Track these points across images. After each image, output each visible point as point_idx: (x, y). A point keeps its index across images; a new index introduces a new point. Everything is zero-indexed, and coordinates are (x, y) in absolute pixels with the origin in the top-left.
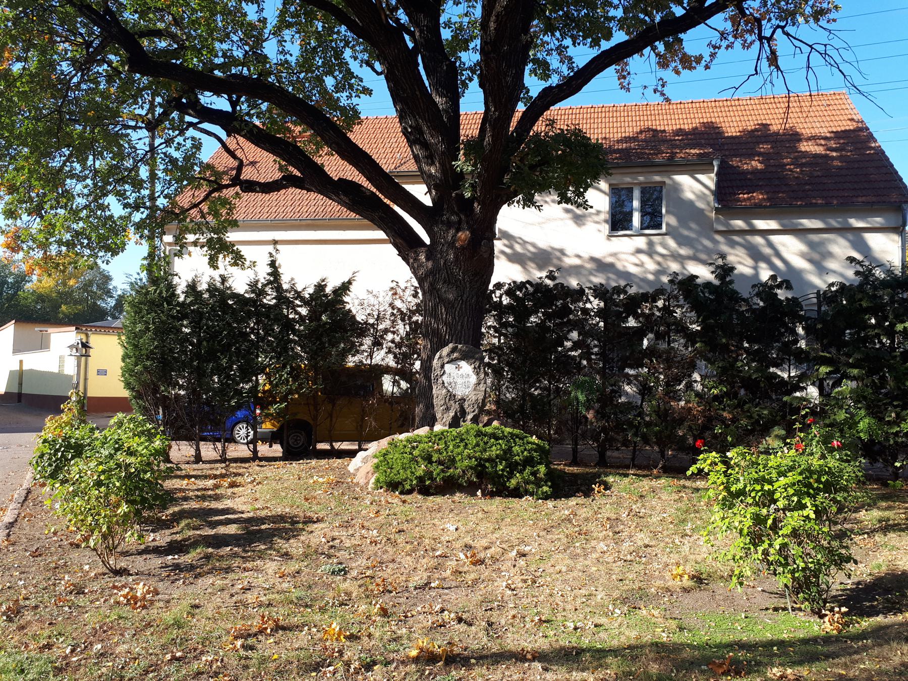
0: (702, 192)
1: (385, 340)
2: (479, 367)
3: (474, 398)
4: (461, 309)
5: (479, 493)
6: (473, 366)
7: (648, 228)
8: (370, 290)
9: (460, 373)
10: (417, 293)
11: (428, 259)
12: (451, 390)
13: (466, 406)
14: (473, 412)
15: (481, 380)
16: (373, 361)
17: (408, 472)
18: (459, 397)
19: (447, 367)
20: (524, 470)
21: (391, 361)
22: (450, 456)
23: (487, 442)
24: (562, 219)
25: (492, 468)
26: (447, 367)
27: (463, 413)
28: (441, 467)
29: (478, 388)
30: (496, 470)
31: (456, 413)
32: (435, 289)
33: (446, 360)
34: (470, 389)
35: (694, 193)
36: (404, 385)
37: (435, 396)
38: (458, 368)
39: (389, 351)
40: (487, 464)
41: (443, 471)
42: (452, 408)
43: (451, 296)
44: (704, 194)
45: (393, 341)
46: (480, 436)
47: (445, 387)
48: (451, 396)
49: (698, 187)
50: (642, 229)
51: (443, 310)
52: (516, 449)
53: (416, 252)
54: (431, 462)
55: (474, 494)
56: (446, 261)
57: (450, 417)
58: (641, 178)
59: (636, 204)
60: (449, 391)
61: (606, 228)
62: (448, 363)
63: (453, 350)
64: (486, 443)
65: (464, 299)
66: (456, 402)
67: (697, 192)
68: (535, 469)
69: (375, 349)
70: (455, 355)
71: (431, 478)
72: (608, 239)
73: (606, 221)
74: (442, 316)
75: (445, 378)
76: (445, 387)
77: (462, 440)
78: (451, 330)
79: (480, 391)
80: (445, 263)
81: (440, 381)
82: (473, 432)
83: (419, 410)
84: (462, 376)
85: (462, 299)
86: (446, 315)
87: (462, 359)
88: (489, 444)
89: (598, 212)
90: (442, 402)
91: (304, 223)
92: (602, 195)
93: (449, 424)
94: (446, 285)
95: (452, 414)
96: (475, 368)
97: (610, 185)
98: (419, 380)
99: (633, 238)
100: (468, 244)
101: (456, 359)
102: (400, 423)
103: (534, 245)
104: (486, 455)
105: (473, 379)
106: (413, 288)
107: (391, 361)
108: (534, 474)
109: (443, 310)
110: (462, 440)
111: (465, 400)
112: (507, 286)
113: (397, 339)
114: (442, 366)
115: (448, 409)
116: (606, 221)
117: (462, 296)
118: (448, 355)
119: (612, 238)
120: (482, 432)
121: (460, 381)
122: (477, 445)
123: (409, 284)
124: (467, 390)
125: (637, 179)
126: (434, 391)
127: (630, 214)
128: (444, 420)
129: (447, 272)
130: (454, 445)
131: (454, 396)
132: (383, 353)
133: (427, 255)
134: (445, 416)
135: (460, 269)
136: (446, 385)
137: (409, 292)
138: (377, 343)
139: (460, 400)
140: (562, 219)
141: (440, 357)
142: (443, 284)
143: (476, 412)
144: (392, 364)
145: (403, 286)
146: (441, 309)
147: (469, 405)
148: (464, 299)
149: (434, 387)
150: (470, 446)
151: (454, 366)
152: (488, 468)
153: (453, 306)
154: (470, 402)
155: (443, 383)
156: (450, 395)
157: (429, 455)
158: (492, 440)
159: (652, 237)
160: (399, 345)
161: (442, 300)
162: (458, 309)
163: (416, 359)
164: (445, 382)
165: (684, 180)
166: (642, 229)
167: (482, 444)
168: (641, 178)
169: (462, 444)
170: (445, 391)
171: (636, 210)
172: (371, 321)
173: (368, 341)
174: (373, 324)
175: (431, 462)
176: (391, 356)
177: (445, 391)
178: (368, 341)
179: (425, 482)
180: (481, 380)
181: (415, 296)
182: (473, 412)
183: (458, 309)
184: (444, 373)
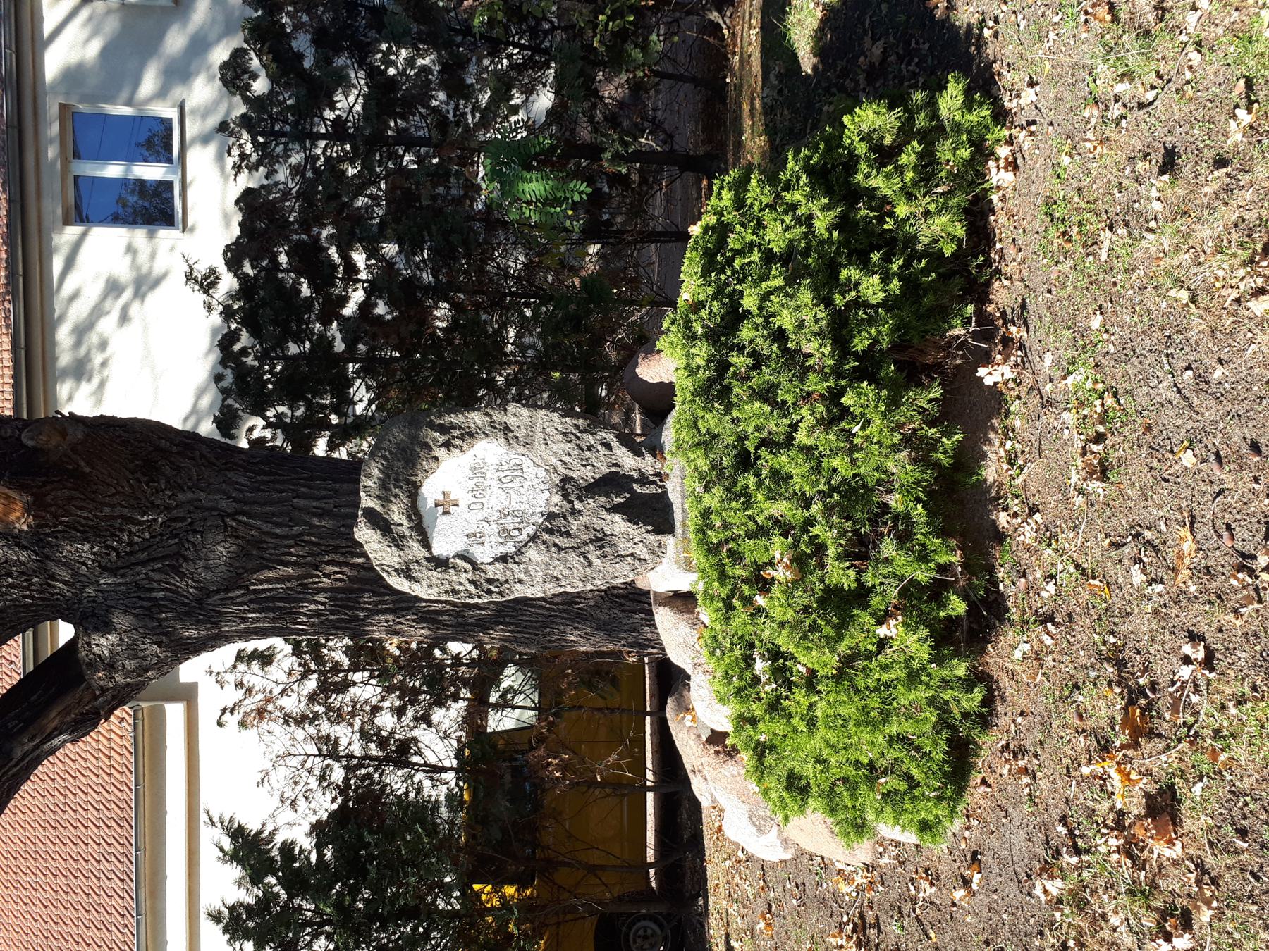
0: (85, 25)
1: (393, 732)
2: (443, 429)
3: (559, 446)
4: (266, 518)
5: (989, 376)
6: (440, 452)
7: (168, 147)
8: (259, 777)
9: (464, 499)
10: (255, 656)
11: (106, 627)
12: (530, 530)
13: (588, 475)
14: (608, 446)
15: (492, 424)
16: (447, 764)
17: (904, 698)
18: (557, 498)
19: (441, 547)
20: (871, 193)
21: (449, 716)
22: (828, 511)
23: (754, 354)
24: (145, 328)
25: (872, 321)
26: (441, 547)
27: (611, 483)
28: (888, 548)
29: (521, 433)
30: (884, 304)
31: (615, 509)
32: (199, 601)
33: (417, 551)
34: (527, 463)
35: (88, 40)
36: (511, 677)
37: (551, 589)
38: (446, 506)
39: (426, 719)
40: (860, 344)
41: (904, 538)
42: (598, 524)
43: (223, 551)
44: (90, 19)
45: (399, 712)
46: (727, 390)
47: (519, 552)
48: (553, 525)
49: (75, 30)
50: (170, 161)
51: (272, 574)
52: (776, 235)
53: (90, 665)
54: (861, 595)
55: (995, 400)
56: (103, 568)
57: (631, 529)
58: (52, 152)
59: (114, 170)
60: (533, 538)
61: (164, 234)
62: (426, 544)
63: (380, 523)
64: (759, 361)
65: (230, 507)
66: (574, 512)
67: (85, 34)
68: (861, 149)
69: (416, 759)
70: (397, 515)
71: (937, 591)
72: (192, 230)
73: (151, 235)
74: (289, 578)
75: (483, 554)
76: (519, 552)
77: (745, 462)
78: (336, 549)
79: (532, 427)
80: (113, 571)
81: (495, 571)
82: (711, 421)
83: (581, 642)
84: (477, 491)
85: (232, 516)
86: (286, 564)
87: (414, 492)
88: (763, 346)
89: (131, 250)
90: (574, 559)
91: (146, 905)
92: (89, 240)
93: (657, 531)
94: (186, 567)
95: (618, 525)
96: (448, 445)
97: (67, 222)
98: (498, 644)
99: (189, 179)
100: (22, 488)
101: (414, 513)
102: (608, 688)
103: (200, 394)
104: (817, 349)
105: (489, 450)
106: (242, 667)
107: (449, 716)
108: (884, 155)
109: (272, 574)
110: (745, 462)
111: (566, 480)
112: (230, 401)
113: (394, 700)
114: (441, 563)
115: (600, 540)
116: (151, 235)
117: (223, 515)
118: (397, 542)
119: (190, 222)
120: (712, 382)
121: (496, 500)
122: (767, 394)
123: (230, 678)
124: (531, 471)
125: (53, 162)
126: (536, 592)
127: (141, 183)
128: (641, 551)
129: (143, 563)
130: (772, 496)
131: (551, 516)
132: (425, 736)
133: (96, 630)
134: (624, 548)
135: (131, 520)
136: (510, 548)
137: (254, 676)
138: (401, 753)
139: (566, 497)
140: (145, 328)
141: (407, 573)
142: (182, 576)
143: (610, 437)
144: (458, 709)
145: (234, 695)
146: (268, 580)
147: (586, 463)
148: (230, 507)
149: (520, 592)
150: (777, 426)
151: (442, 521)
152: (876, 341)
153: (257, 543)
154: (576, 463)
155: (503, 559)
156: (550, 531)
157: (822, 602)
158: (746, 332)
159: (188, 135)
160: (410, 696)
161: (236, 578)
162: (267, 527)
163: (444, 650)
164: (501, 550)
165: (54, 61)
166: (170, 161)
167: (766, 375)
168: (52, 152)
169: (768, 460)
170: (532, 553)
171: (128, 170)
172: (338, 774)
173: (395, 780)
174: (348, 769)
175: (861, 595)
176: (438, 715)
177: (532, 553)
178: (395, 780)
179: (952, 621)
180: (492, 424)
181: (265, 659)
182: (608, 446)
183: (267, 527)
184: (464, 557)
